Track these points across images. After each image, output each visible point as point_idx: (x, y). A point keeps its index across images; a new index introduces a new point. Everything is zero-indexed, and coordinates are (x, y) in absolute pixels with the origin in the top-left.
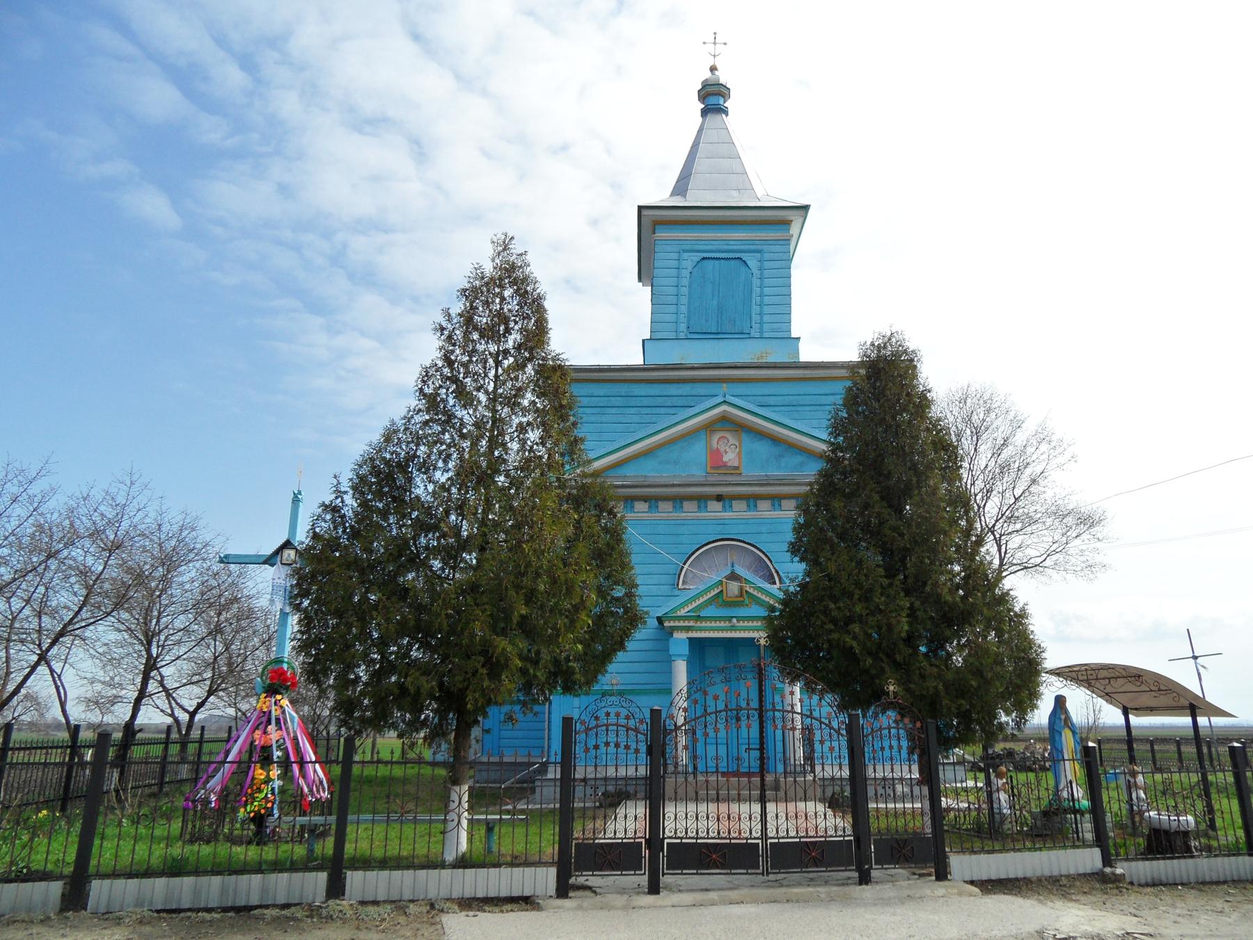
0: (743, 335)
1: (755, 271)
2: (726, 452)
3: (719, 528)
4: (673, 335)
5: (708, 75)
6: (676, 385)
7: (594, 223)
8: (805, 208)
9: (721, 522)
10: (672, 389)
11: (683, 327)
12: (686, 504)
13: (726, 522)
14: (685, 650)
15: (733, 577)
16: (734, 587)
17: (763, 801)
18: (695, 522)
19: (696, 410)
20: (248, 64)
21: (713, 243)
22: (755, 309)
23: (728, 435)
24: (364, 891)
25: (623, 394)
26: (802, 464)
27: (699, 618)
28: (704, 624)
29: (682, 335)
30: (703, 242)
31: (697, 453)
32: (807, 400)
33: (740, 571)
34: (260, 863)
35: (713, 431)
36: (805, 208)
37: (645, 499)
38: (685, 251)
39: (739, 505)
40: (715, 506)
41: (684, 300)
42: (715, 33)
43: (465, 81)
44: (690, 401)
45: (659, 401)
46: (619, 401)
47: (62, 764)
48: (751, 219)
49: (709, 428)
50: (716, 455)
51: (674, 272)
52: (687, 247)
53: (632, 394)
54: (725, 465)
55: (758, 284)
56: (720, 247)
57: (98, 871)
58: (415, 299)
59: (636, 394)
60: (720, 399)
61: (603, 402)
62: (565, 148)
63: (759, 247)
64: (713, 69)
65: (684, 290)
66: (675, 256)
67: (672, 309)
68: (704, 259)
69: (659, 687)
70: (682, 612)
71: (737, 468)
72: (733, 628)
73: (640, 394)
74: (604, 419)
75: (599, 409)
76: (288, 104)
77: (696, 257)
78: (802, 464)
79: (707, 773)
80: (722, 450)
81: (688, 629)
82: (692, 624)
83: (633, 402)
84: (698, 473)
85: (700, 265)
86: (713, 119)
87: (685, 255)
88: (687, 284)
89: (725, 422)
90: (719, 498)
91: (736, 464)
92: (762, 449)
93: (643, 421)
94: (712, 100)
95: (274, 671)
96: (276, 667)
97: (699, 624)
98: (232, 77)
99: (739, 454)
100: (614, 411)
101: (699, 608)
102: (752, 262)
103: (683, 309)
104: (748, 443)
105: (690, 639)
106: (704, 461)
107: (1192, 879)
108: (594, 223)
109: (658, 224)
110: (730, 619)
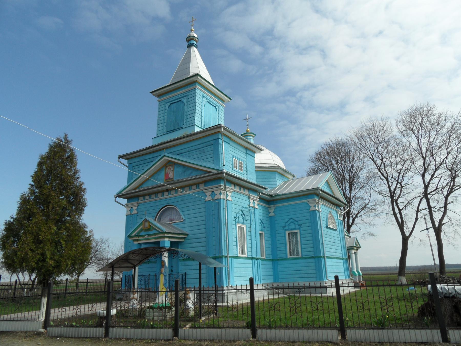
0: (181, 128)
2: (170, 173)
3: (167, 202)
6: (157, 153)
7: (398, 59)
13: (169, 199)
15: (146, 220)
16: (147, 224)
17: (247, 302)
20: (262, 44)
21: (174, 97)
24: (234, 337)
25: (143, 159)
26: (191, 173)
27: (139, 236)
31: (162, 175)
32: (194, 148)
33: (148, 218)
34: (265, 325)
35: (166, 167)
40: (166, 193)
43: (336, 21)
44: (152, 159)
46: (142, 162)
47: (218, 290)
48: (183, 85)
56: (176, 98)
57: (35, 319)
58: (328, 109)
59: (146, 158)
62: (381, 33)
63: (186, 94)
70: (133, 235)
71: (172, 179)
72: (148, 239)
75: (138, 166)
76: (276, 53)
77: (169, 104)
78: (191, 173)
79: (232, 292)
80: (169, 173)
81: (137, 240)
82: (137, 238)
90: (167, 190)
97: (140, 238)
98: (258, 49)
100: (142, 166)
107: (287, 340)
108: (398, 59)
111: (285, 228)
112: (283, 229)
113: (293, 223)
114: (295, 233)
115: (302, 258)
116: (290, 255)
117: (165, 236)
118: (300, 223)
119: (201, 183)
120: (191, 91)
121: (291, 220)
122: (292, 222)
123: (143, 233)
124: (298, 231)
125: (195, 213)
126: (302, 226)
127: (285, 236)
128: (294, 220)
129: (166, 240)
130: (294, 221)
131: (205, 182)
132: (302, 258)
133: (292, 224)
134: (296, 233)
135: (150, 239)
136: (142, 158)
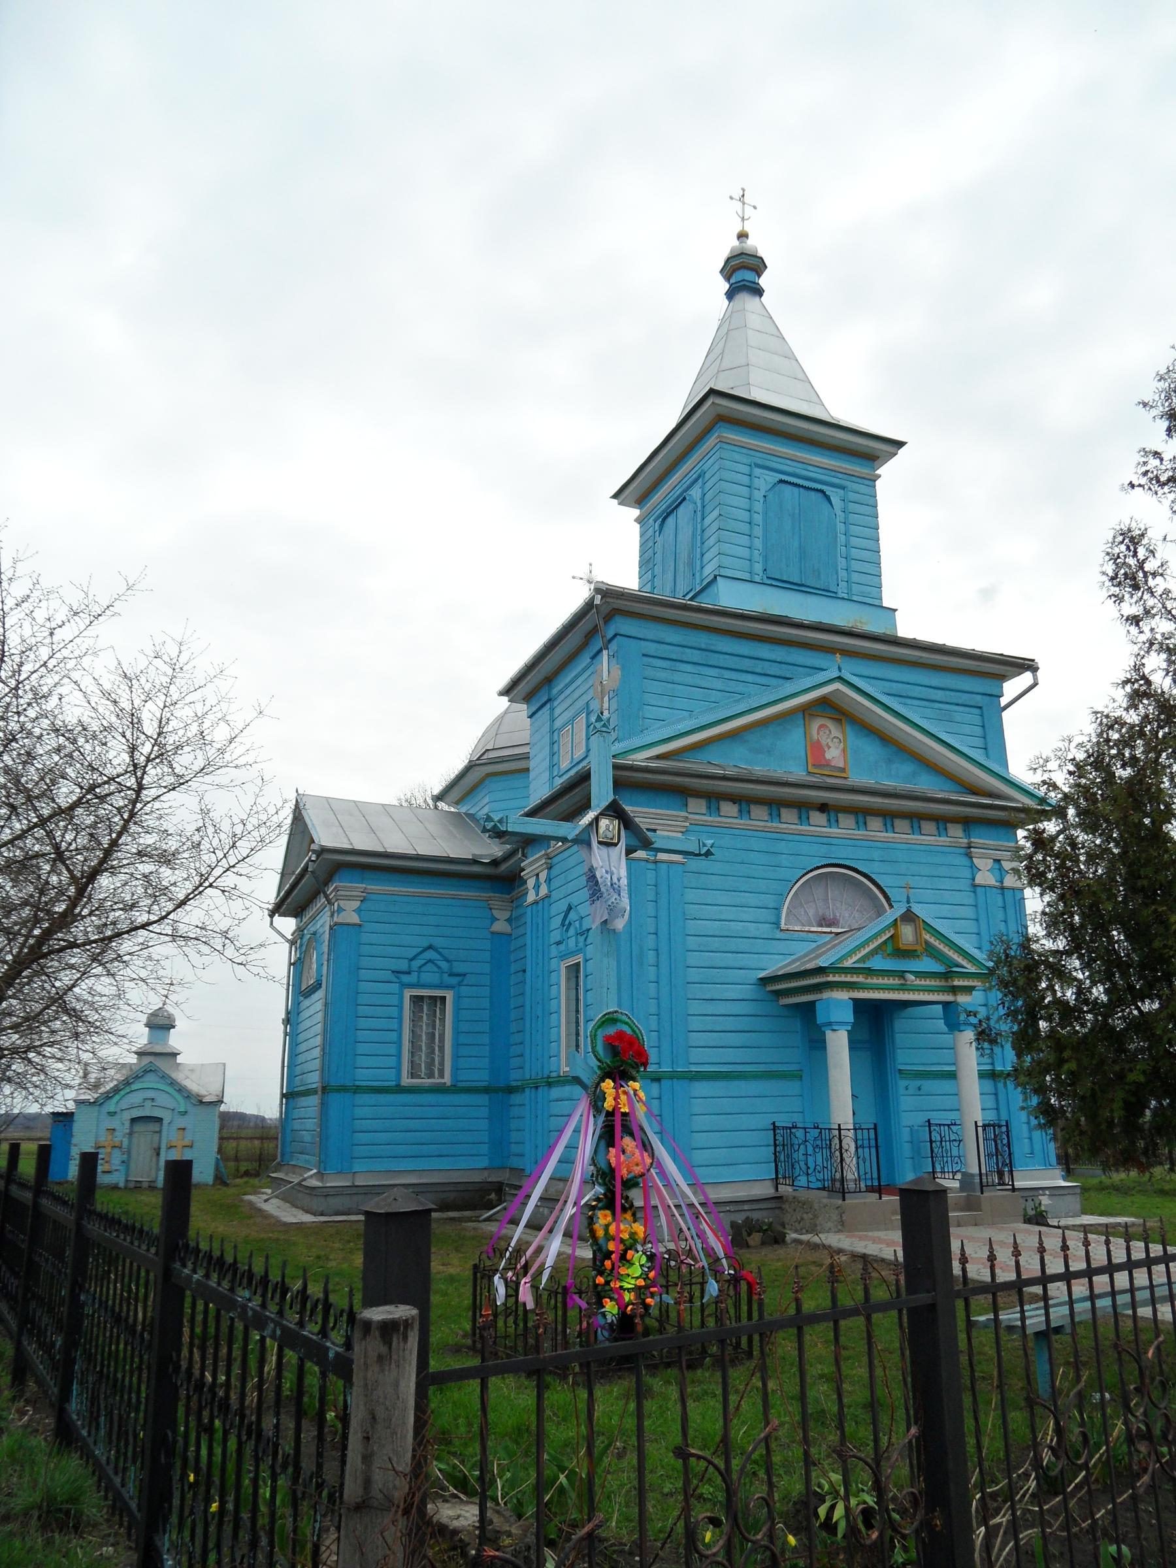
0: (828, 593)
1: (839, 513)
3: (823, 850)
4: (746, 576)
5: (736, 243)
6: (785, 648)
8: (900, 444)
9: (825, 840)
10: (764, 651)
11: (758, 568)
12: (785, 812)
14: (847, 1015)
18: (797, 838)
19: (790, 688)
22: (842, 563)
23: (830, 724)
25: (703, 646)
27: (869, 972)
28: (875, 981)
29: (757, 579)
30: (779, 460)
31: (794, 741)
36: (900, 444)
37: (734, 799)
38: (758, 466)
39: (847, 821)
40: (818, 818)
41: (758, 531)
42: (743, 190)
45: (746, 664)
46: (696, 656)
49: (808, 711)
50: (816, 750)
51: (744, 491)
52: (760, 462)
53: (713, 648)
54: (827, 764)
55: (843, 531)
56: (798, 471)
59: (719, 648)
60: (836, 674)
61: (675, 653)
64: (742, 236)
65: (758, 518)
66: (746, 469)
67: (744, 540)
68: (781, 481)
69: (762, 1068)
70: (848, 963)
71: (843, 770)
72: (903, 988)
73: (724, 650)
74: (677, 677)
80: (824, 743)
83: (714, 659)
84: (796, 771)
85: (777, 488)
86: (746, 301)
87: (757, 471)
88: (760, 510)
89: (829, 708)
90: (823, 808)
91: (841, 765)
92: (870, 749)
93: (727, 689)
94: (739, 276)
95: (608, 1040)
96: (611, 1031)
99: (844, 751)
100: (689, 668)
101: (863, 959)
102: (835, 496)
103: (758, 543)
104: (854, 739)
105: (856, 1001)
106: (803, 754)
109: (723, 419)
110: (901, 974)
111: (406, 979)
112: (395, 980)
113: (436, 965)
114: (433, 999)
115: (454, 1089)
116: (413, 1075)
117: (828, 982)
118: (460, 968)
119: (955, 820)
120: (854, 479)
121: (431, 954)
122: (430, 961)
123: (878, 963)
124: (449, 996)
125: (760, 905)
126: (469, 980)
127: (400, 1007)
128: (440, 954)
129: (843, 996)
130: (438, 957)
131: (967, 823)
132: (454, 1089)
133: (430, 967)
134: (443, 999)
135: (908, 990)
136: (702, 639)
